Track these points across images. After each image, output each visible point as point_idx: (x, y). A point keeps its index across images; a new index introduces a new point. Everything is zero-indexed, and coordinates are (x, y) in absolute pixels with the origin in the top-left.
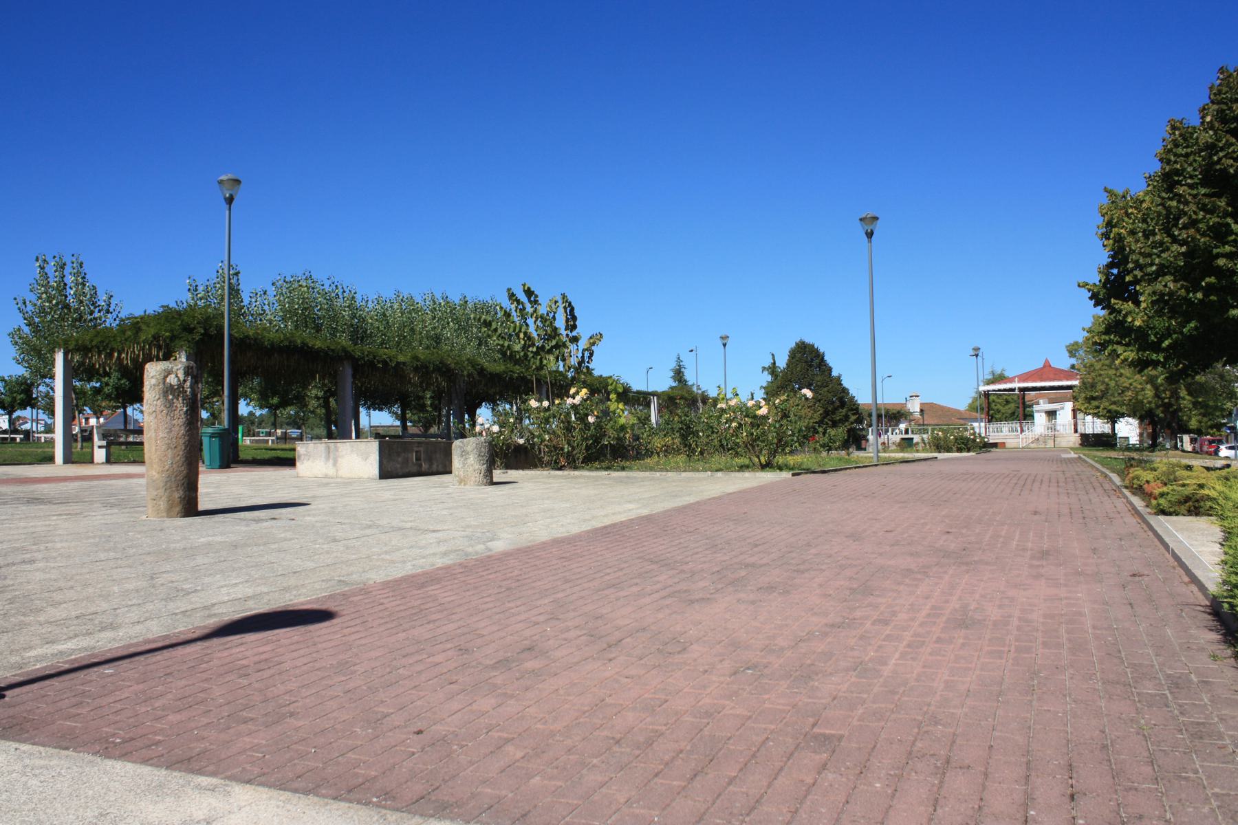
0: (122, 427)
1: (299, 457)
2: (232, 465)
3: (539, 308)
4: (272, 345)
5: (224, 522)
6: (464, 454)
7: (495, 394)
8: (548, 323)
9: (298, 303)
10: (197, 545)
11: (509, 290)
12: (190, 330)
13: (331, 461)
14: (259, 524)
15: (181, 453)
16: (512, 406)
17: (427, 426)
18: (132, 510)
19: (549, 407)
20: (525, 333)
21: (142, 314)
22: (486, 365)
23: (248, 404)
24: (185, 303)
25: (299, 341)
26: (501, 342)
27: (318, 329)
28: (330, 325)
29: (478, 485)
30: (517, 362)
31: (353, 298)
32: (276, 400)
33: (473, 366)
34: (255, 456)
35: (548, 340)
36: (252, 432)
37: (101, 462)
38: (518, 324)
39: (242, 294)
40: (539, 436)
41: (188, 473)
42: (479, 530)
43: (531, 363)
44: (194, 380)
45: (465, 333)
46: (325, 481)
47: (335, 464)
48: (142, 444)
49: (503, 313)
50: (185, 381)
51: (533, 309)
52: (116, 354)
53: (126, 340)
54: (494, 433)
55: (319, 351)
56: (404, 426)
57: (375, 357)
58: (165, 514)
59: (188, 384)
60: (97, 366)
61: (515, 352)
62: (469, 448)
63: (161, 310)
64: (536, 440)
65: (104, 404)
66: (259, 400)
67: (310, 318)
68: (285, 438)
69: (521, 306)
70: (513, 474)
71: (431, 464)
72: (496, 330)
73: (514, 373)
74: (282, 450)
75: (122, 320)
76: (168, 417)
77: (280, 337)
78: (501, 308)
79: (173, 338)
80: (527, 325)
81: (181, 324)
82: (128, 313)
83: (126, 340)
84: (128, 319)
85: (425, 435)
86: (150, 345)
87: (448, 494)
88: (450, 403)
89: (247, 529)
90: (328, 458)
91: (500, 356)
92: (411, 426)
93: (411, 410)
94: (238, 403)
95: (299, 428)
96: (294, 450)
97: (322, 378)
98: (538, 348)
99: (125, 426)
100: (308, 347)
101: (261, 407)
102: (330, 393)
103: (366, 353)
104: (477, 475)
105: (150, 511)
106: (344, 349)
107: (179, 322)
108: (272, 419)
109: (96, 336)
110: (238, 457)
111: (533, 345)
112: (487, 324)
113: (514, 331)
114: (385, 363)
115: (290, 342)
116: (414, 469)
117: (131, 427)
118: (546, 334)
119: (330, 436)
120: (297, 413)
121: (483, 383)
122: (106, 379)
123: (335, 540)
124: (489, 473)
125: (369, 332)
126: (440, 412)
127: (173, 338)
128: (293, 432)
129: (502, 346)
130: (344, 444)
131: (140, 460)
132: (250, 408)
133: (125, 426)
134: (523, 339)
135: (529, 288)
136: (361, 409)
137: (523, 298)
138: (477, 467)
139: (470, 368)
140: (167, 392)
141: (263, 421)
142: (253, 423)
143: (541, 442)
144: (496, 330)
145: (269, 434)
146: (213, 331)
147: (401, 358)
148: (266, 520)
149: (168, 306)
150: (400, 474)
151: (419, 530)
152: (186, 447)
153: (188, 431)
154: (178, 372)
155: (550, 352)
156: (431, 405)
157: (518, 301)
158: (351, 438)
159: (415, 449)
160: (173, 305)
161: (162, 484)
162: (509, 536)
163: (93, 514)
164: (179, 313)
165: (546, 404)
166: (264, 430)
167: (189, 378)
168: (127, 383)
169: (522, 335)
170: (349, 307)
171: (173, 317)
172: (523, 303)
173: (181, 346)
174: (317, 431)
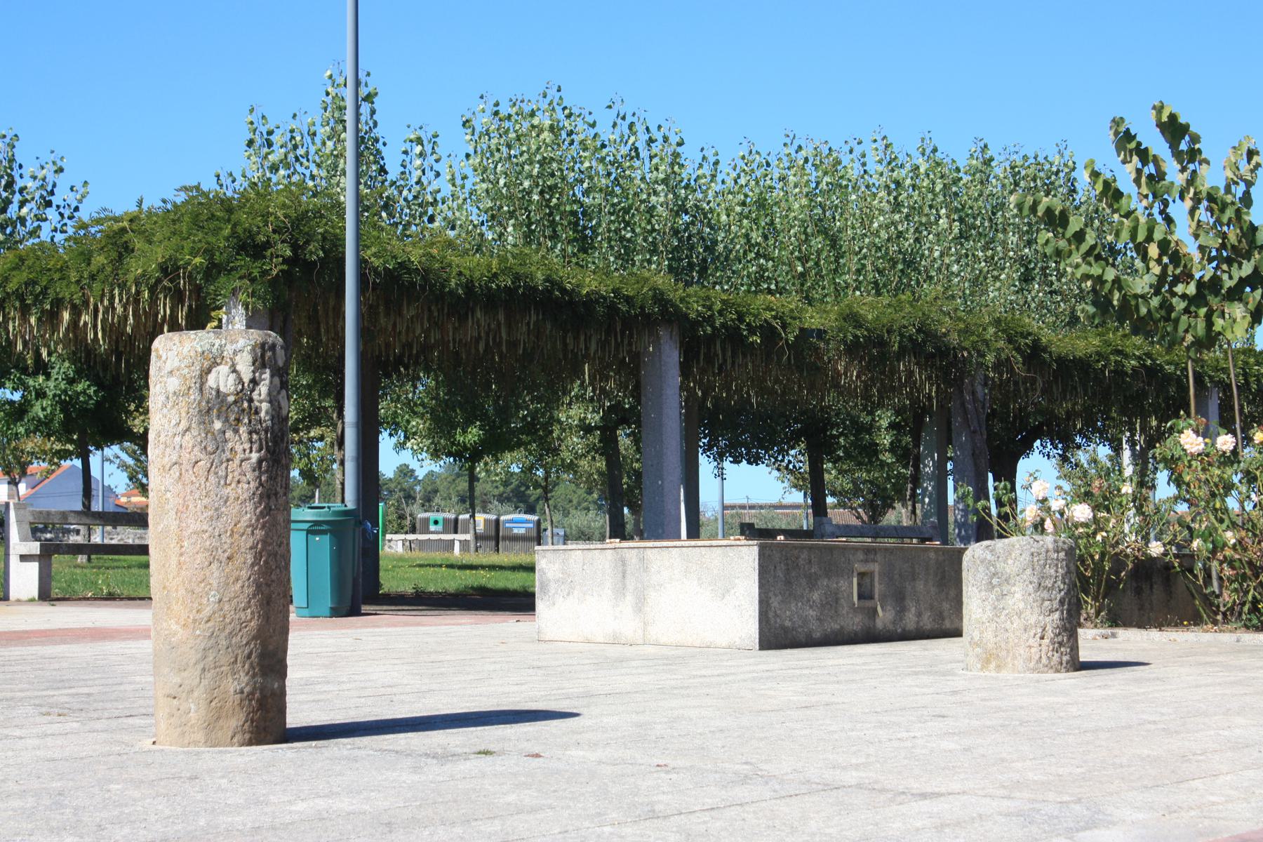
0: (79, 507)
1: (544, 587)
2: (365, 608)
3: (1203, 170)
4: (469, 286)
5: (355, 760)
6: (997, 581)
7: (1070, 415)
8: (1229, 213)
9: (530, 176)
10: (288, 819)
11: (1117, 122)
12: (252, 248)
13: (630, 598)
14: (449, 766)
15: (244, 574)
16: (1117, 449)
17: (878, 503)
18: (114, 723)
19: (1235, 452)
20: (1164, 245)
21: (133, 208)
22: (1047, 335)
23: (401, 446)
24: (240, 179)
25: (540, 276)
26: (1096, 270)
27: (585, 244)
28: (617, 231)
29: (1033, 670)
30: (1142, 326)
31: (676, 155)
32: (473, 435)
33: (1010, 340)
34: (422, 585)
35: (1229, 261)
36: (408, 522)
37: (24, 597)
38: (1143, 220)
39: (385, 152)
40: (1209, 535)
41: (260, 629)
42: (1051, 796)
43: (1182, 327)
44: (277, 380)
45: (985, 249)
46: (613, 651)
47: (640, 604)
48: (143, 550)
49: (1099, 187)
50: (254, 382)
51: (1186, 175)
52: (66, 316)
53: (93, 277)
54: (1076, 526)
55: (592, 301)
56: (819, 508)
57: (741, 318)
58: (200, 736)
59: (263, 389)
60: (20, 347)
61: (1136, 296)
62: (1010, 567)
63: (181, 198)
64: (1196, 544)
65: (29, 446)
66: (430, 433)
67: (562, 214)
68: (495, 536)
69: (1150, 169)
70: (1130, 642)
71: (901, 610)
72: (1079, 237)
73: (1126, 356)
74: (492, 567)
75: (84, 226)
76: (212, 478)
77: (489, 266)
78: (1095, 175)
79: (213, 270)
80: (1169, 220)
81: (234, 232)
82: (97, 208)
83: (93, 277)
84: (98, 221)
85: (873, 528)
86: (152, 290)
87: (954, 693)
88: (947, 438)
89: (416, 778)
90: (620, 591)
91: (1091, 309)
92: (835, 507)
93: (836, 461)
94: (377, 442)
95: (531, 510)
96: (530, 569)
97: (600, 375)
98: (1200, 284)
99: (87, 505)
100: (563, 290)
101: (436, 455)
102: (616, 418)
103: (718, 306)
104: (1034, 642)
105: (163, 726)
106: (659, 297)
107: (227, 232)
108: (463, 485)
109: (16, 268)
110: (378, 585)
111: (1187, 276)
112: (1057, 220)
113: (1133, 237)
114: (769, 332)
115: (517, 277)
116: (855, 623)
117: (97, 506)
118: (1223, 246)
119: (618, 531)
120: (528, 470)
121: (1039, 384)
122: (41, 378)
123: (653, 815)
124: (1069, 629)
125: (721, 247)
126: (916, 468)
127: (213, 270)
128: (518, 521)
129: (1099, 280)
130: (665, 552)
131: (142, 594)
132: (406, 457)
133: (87, 505)
134: (1159, 261)
135: (1173, 117)
136: (703, 459)
137: (1157, 144)
138: (1032, 620)
139: (1001, 344)
140: (209, 410)
141: (436, 491)
142: (409, 497)
143: (1214, 552)
144: (1079, 237)
145: (454, 526)
146: (314, 252)
147: (813, 319)
148: (465, 757)
149: (197, 188)
150: (817, 635)
151: (882, 791)
152: (258, 557)
153: (262, 515)
154: (238, 358)
155: (1235, 294)
156: (893, 449)
157: (1143, 154)
158: (678, 537)
159: (859, 567)
160: (209, 185)
161: (193, 656)
162: (1141, 816)
163: (18, 733)
164: (227, 206)
165: (1225, 442)
166: (440, 516)
167: (267, 375)
168: (91, 391)
169: (1153, 251)
170: (665, 181)
171: (212, 217)
172: (1156, 160)
173: (234, 292)
174: (579, 519)
